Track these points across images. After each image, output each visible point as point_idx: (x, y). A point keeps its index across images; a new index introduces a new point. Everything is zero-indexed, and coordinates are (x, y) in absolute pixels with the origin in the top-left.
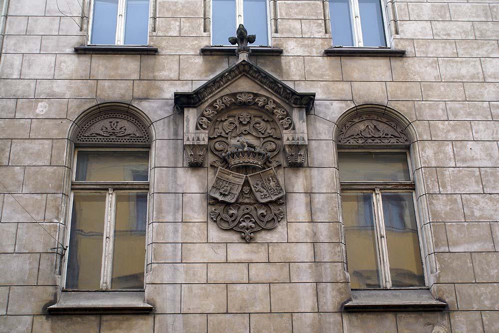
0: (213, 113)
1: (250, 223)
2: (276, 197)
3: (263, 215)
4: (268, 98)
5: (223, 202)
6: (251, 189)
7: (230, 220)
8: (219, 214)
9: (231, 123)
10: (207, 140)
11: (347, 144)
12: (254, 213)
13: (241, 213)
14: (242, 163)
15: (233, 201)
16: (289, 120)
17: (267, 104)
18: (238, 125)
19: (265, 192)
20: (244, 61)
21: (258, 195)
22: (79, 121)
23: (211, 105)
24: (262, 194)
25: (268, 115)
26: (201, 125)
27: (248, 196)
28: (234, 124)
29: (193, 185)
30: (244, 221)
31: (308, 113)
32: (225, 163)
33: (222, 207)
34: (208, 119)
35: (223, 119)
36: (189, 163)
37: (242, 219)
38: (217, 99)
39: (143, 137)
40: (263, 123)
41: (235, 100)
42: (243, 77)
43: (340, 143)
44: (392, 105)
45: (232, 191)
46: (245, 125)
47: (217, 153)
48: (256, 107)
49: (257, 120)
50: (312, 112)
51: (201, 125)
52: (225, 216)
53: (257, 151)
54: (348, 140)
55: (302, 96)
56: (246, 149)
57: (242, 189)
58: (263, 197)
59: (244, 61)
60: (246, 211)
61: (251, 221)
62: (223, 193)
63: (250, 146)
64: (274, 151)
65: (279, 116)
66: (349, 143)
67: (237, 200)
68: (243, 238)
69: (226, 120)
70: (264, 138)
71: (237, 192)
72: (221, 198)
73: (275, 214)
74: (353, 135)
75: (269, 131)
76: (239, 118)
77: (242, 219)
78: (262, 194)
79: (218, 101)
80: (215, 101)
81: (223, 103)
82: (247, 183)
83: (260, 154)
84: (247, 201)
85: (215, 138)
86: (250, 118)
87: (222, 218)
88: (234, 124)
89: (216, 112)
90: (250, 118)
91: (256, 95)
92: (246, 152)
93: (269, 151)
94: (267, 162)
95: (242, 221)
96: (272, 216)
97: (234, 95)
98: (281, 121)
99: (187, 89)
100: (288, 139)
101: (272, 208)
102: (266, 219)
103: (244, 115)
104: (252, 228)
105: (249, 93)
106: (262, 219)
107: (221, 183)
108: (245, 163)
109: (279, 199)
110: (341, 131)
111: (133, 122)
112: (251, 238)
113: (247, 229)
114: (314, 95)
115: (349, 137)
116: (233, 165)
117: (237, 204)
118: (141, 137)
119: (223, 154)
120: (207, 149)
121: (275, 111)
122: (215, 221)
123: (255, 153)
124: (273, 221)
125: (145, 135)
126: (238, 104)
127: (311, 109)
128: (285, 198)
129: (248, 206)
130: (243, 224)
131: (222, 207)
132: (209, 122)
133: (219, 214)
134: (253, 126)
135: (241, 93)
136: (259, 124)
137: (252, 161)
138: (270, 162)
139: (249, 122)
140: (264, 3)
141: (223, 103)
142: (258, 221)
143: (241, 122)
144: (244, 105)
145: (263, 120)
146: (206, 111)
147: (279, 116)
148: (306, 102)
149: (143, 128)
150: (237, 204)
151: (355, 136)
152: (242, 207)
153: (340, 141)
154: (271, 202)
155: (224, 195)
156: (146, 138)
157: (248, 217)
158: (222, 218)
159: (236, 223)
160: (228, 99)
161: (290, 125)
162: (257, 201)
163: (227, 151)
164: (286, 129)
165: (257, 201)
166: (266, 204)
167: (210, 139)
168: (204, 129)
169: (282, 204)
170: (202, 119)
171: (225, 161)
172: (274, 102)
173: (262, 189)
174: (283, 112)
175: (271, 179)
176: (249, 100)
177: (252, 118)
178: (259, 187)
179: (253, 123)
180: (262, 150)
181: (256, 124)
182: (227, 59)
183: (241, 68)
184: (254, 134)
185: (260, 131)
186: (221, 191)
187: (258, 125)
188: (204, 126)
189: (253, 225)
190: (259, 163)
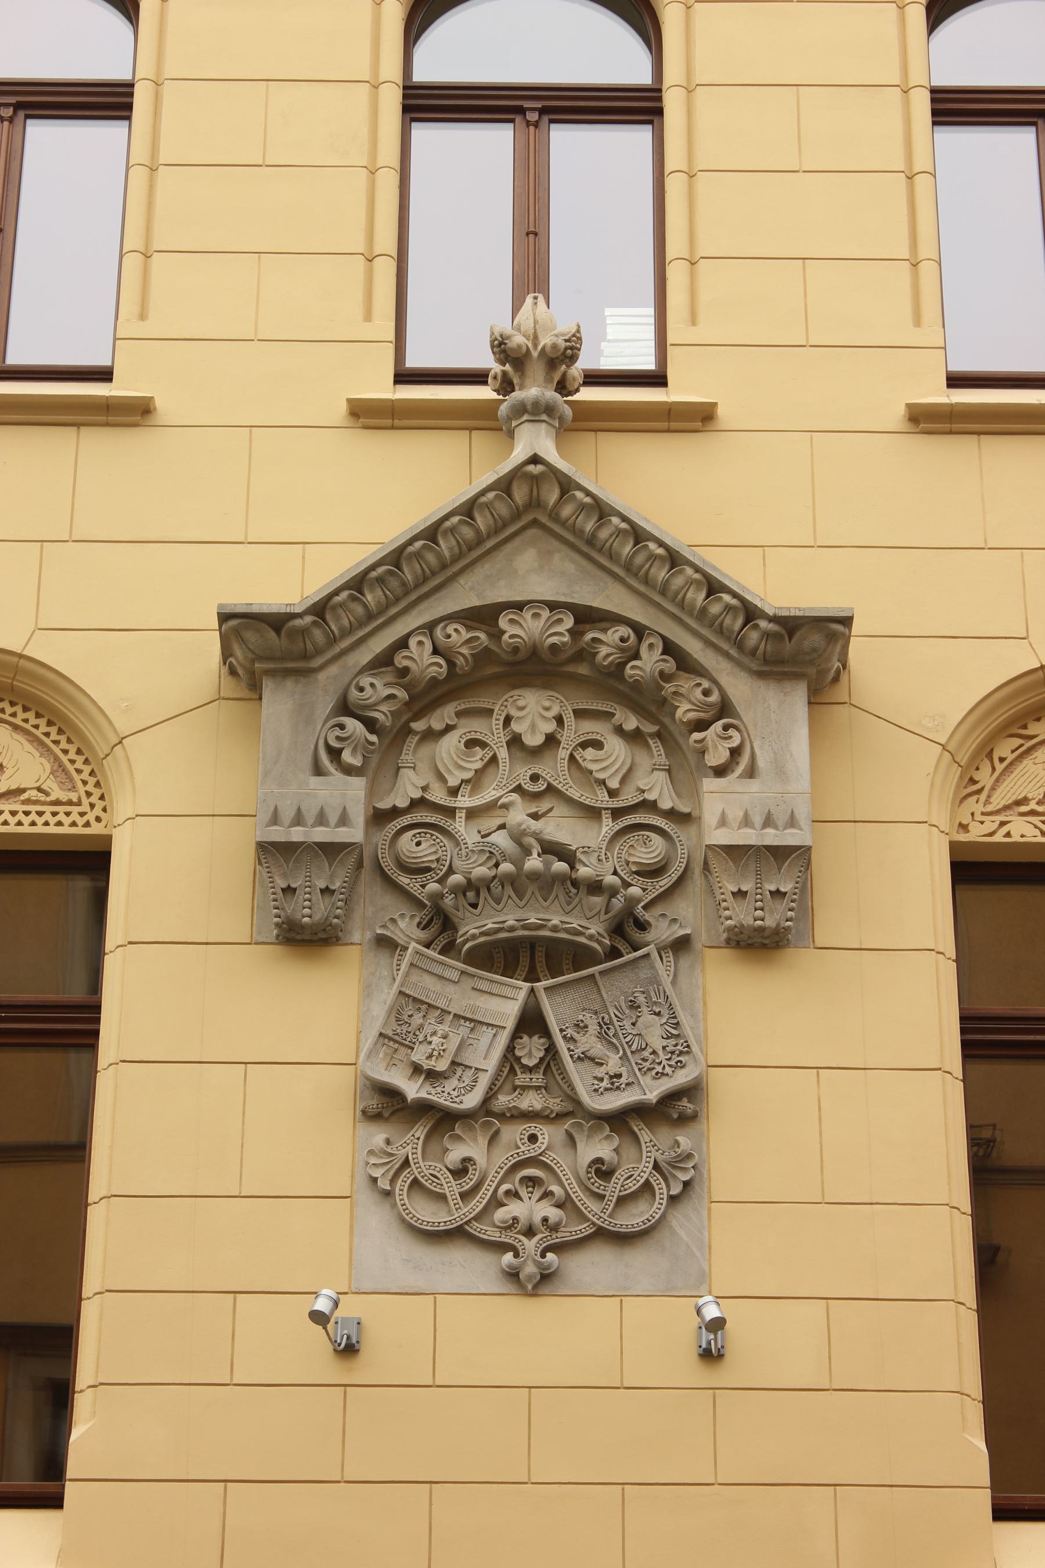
0: (391, 697)
1: (544, 1203)
2: (666, 1085)
3: (603, 1171)
4: (640, 631)
5: (424, 1109)
6: (551, 1050)
7: (452, 1188)
8: (406, 1163)
9: (471, 744)
10: (359, 816)
11: (998, 838)
12: (559, 1158)
13: (503, 1158)
14: (512, 929)
15: (471, 1101)
16: (731, 732)
17: (636, 656)
18: (503, 754)
19: (613, 1063)
20: (535, 459)
21: (581, 1080)
22: (963, 741)
23: (384, 661)
24: (600, 1072)
25: (649, 712)
26: (335, 754)
27: (538, 1079)
28: (483, 745)
29: (329, 1017)
30: (514, 1195)
31: (816, 698)
32: (435, 928)
33: (420, 1131)
34: (370, 724)
35: (437, 726)
36: (277, 925)
37: (505, 1187)
38: (408, 636)
39: (79, 803)
40: (616, 749)
41: (490, 635)
42: (532, 532)
43: (963, 837)
44: (47, 651)
45: (470, 1058)
46: (535, 753)
47: (404, 880)
48: (491, 670)
49: (591, 728)
50: (840, 693)
51: (335, 754)
52: (422, 1168)
53: (583, 871)
54: (1003, 824)
55: (791, 625)
56: (534, 863)
57: (510, 1049)
58: (605, 1084)
59: (535, 459)
60: (528, 1150)
61: (547, 1195)
62: (426, 1065)
63: (552, 849)
64: (654, 872)
65: (684, 711)
66: (1008, 835)
67: (487, 1100)
68: (513, 1275)
69: (449, 728)
70: (617, 813)
71: (487, 1055)
72: (413, 1090)
73: (656, 1166)
74: (1024, 801)
75: (641, 780)
76: (508, 720)
77: (505, 1187)
78: (600, 1072)
79: (413, 642)
80: (402, 643)
81: (436, 651)
82: (531, 1022)
83: (595, 887)
84: (531, 1101)
85: (395, 812)
86: (559, 720)
87: (415, 1183)
88: (483, 745)
89: (402, 694)
90: (559, 720)
91: (587, 617)
92: (534, 876)
93: (637, 873)
94: (627, 928)
95: (508, 1193)
96: (644, 1171)
97: (483, 617)
98: (696, 736)
99: (287, 585)
100: (723, 822)
101: (645, 1136)
102: (613, 1189)
103: (534, 712)
104: (555, 1228)
105: (553, 606)
106: (597, 1185)
107: (417, 1019)
108: (525, 927)
109: (672, 1097)
110: (973, 781)
111: (38, 733)
112: (546, 1277)
113: (530, 1232)
114: (847, 621)
115: (1006, 808)
116: (474, 937)
117: (486, 1115)
118: (70, 803)
119: (433, 887)
120: (360, 865)
121: (669, 688)
122: (388, 1194)
123: (575, 883)
124: (647, 1196)
125: (89, 794)
126: (504, 656)
127: (836, 679)
128: (692, 1091)
129: (533, 1128)
130: (514, 1209)
131: (420, 1131)
132: (374, 738)
133: (406, 1163)
134: (572, 757)
135: (519, 606)
136: (597, 745)
137: (555, 918)
138: (643, 926)
139: (551, 740)
140: (45, 140)
141: (436, 651)
142: (579, 1196)
143: (515, 742)
144: (533, 668)
145: (619, 731)
146: (361, 690)
147: (684, 711)
148: (805, 652)
149: (80, 759)
150: (486, 1115)
151: (1033, 806)
152: (513, 1133)
153: (964, 827)
154: (640, 1111)
155: (432, 1076)
156: (92, 806)
157: (530, 1174)
158: (415, 1183)
159: (478, 1203)
160: (457, 635)
161: (735, 753)
162: (577, 1102)
163: (451, 871)
164: (720, 771)
165: (574, 1110)
166: (619, 1121)
167: (380, 817)
168: (349, 770)
169: (685, 1120)
170: (342, 727)
171: (440, 925)
172: (670, 648)
173: (598, 1049)
174: (706, 693)
175: (641, 999)
176: (554, 639)
177: (569, 719)
178: (590, 1042)
179: (569, 738)
180: (609, 867)
181: (584, 745)
182: (75, 434)
183: (520, 494)
184: (575, 793)
185: (603, 782)
186: (419, 1055)
187: (590, 753)
188: (347, 756)
189: (554, 1214)
190: (589, 926)
